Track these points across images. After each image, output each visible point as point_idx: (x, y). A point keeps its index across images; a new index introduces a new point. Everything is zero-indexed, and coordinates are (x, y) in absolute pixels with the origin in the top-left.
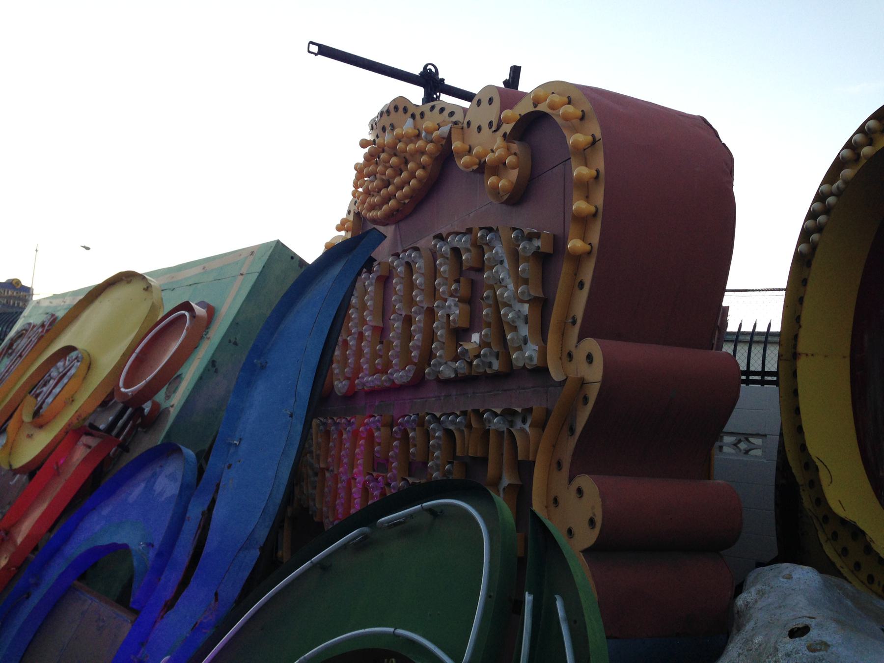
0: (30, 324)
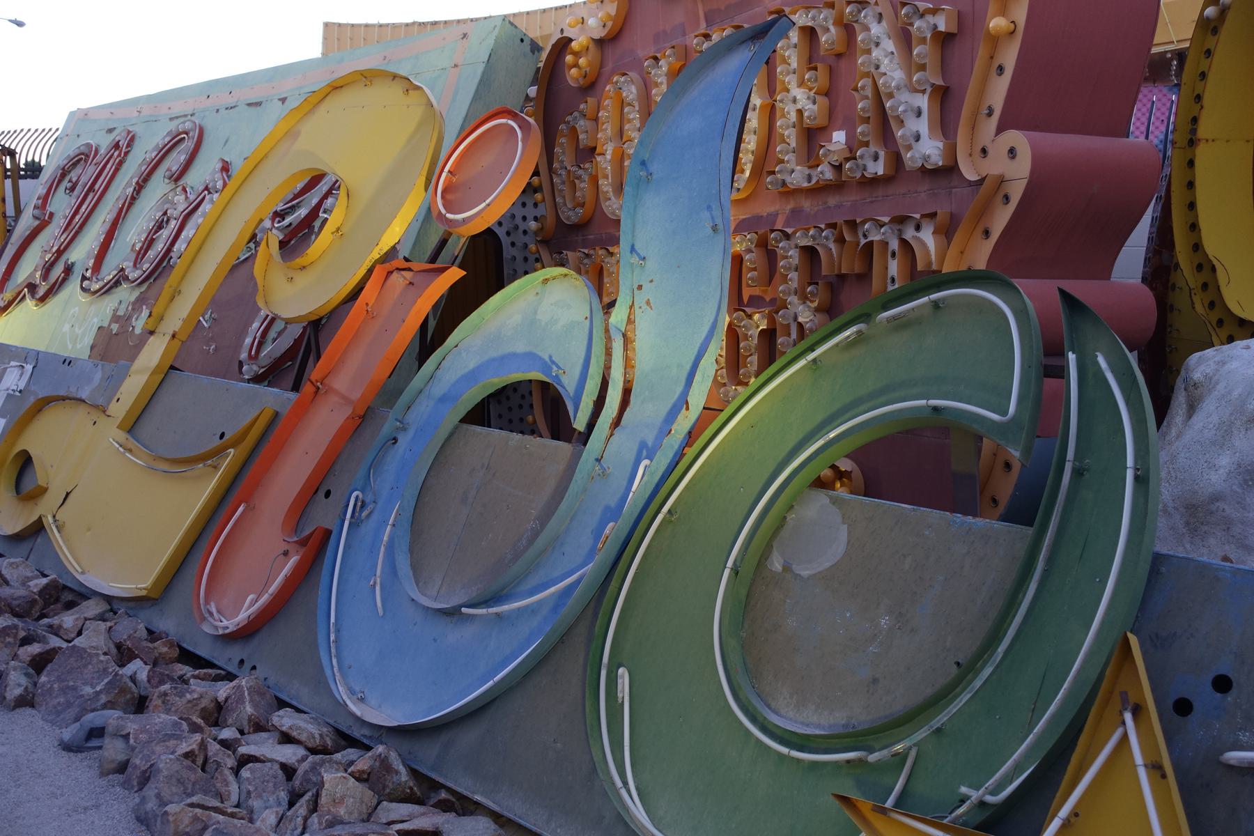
0: (89, 146)
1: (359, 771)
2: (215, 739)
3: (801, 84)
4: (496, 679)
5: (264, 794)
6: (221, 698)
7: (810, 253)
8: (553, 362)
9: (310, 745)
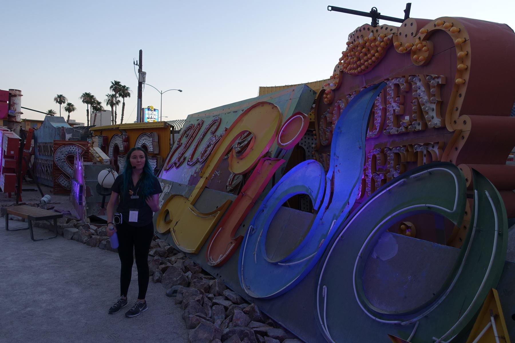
0: (192, 124)
1: (246, 311)
2: (207, 297)
3: (395, 102)
4: (287, 286)
5: (218, 315)
6: (210, 285)
7: (397, 155)
8: (310, 188)
9: (233, 301)
